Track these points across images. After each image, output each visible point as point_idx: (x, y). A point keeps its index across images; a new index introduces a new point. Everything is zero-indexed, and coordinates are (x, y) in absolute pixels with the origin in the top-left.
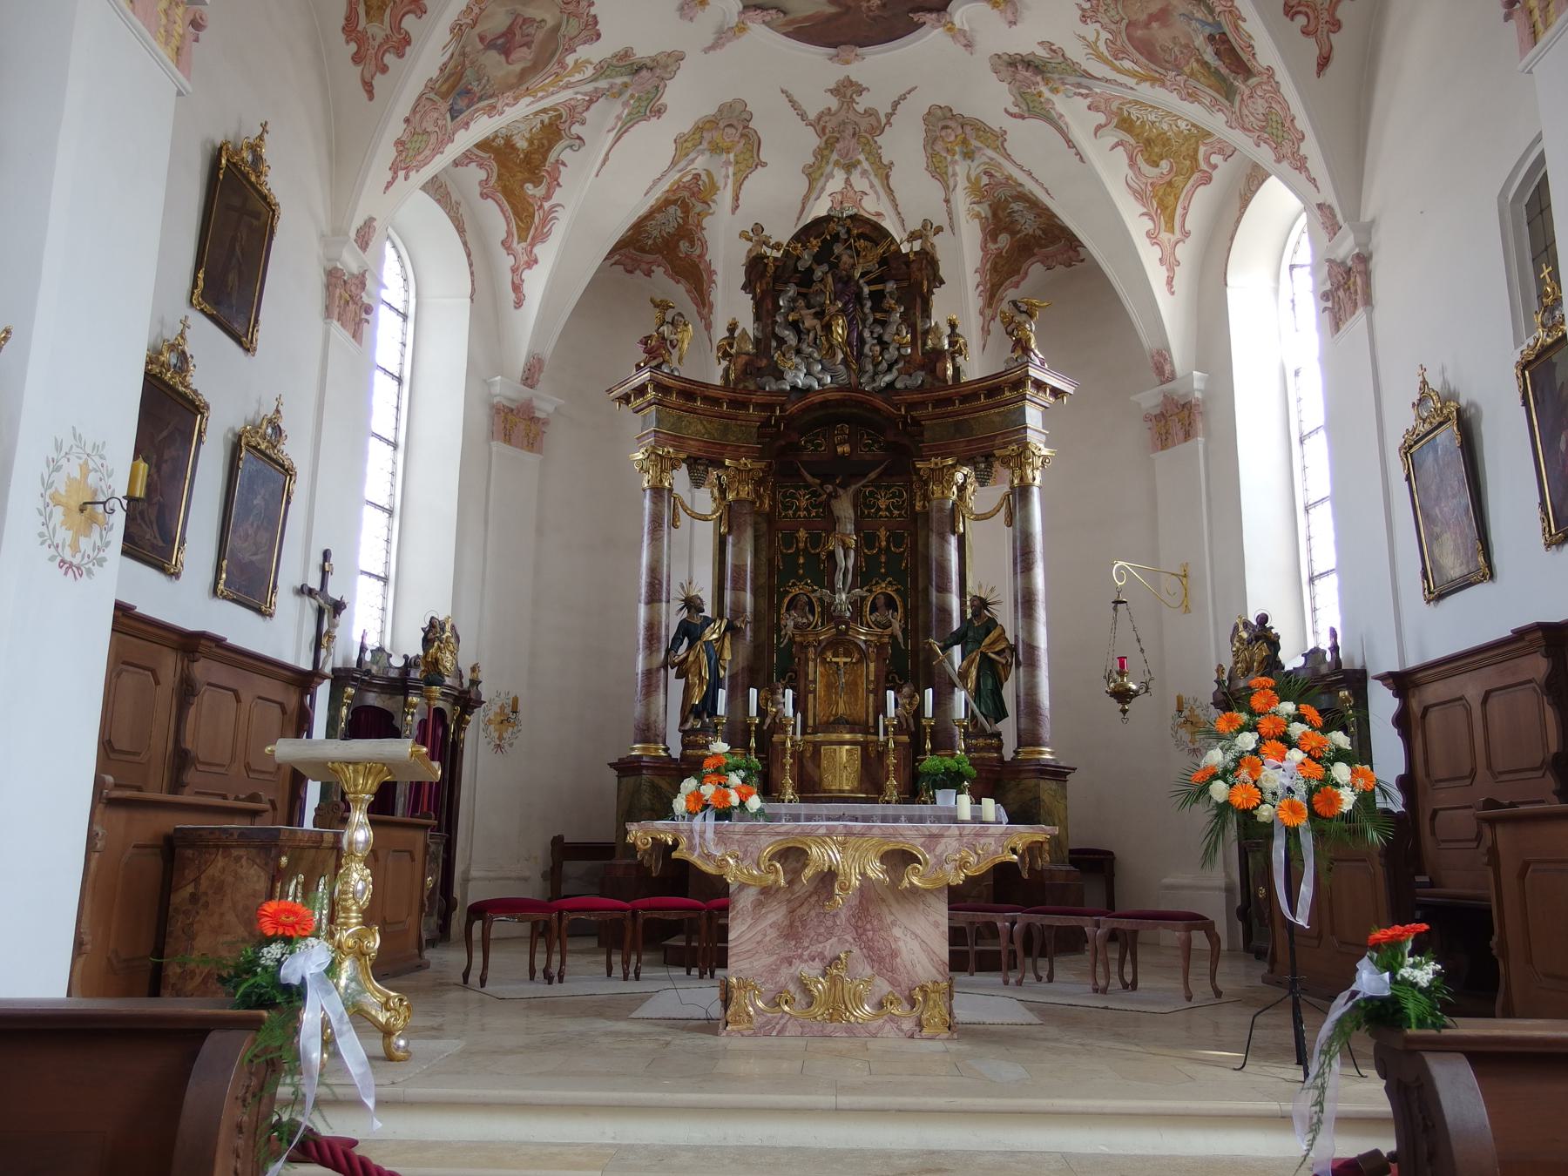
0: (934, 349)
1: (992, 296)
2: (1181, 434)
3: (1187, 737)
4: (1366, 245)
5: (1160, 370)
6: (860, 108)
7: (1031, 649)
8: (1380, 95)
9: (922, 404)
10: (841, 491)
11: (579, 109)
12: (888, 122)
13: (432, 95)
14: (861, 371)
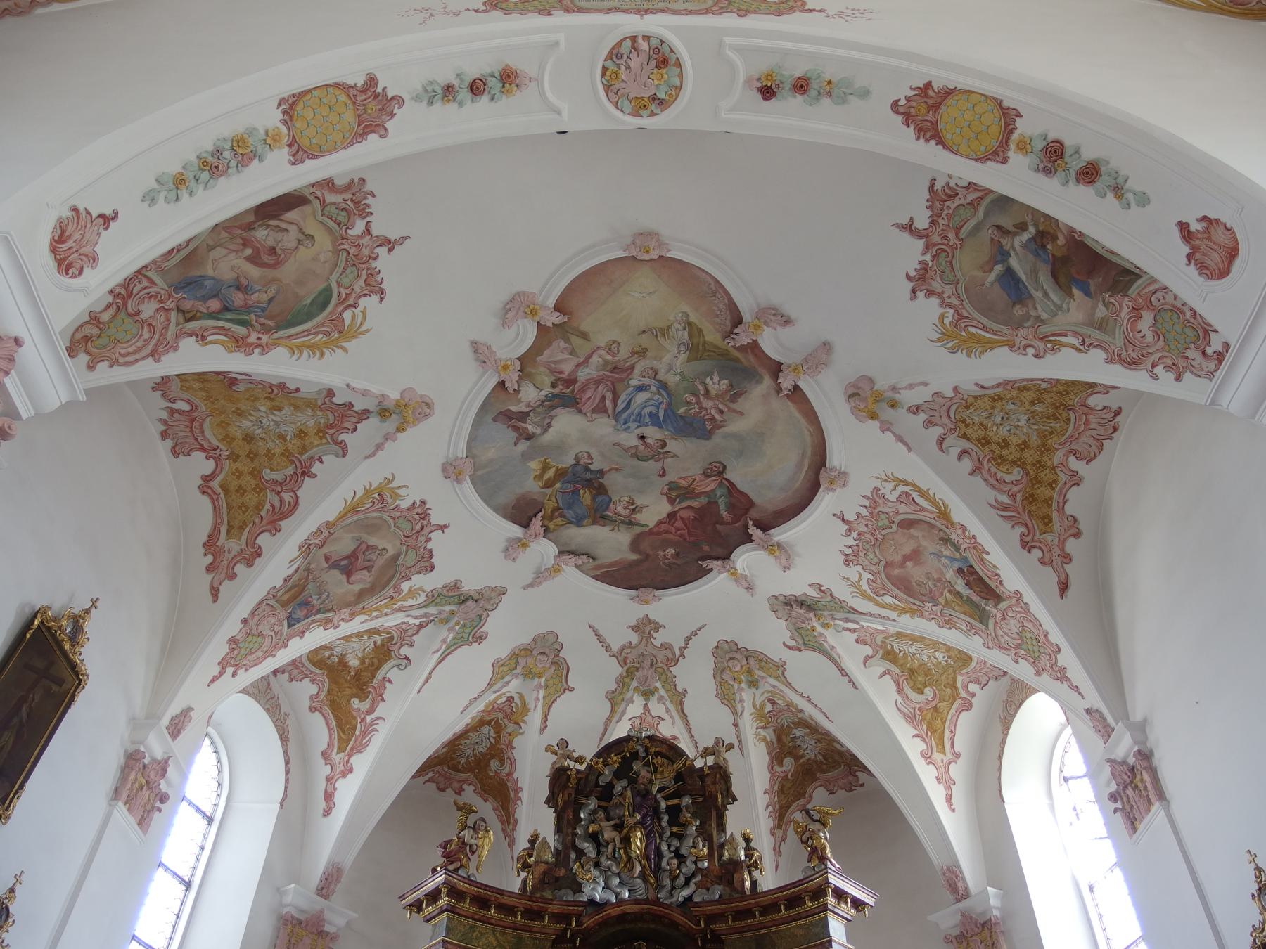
0: (730, 860)
4: (1144, 743)
5: (954, 888)
6: (657, 643)
8: (1122, 613)
9: (721, 916)
11: (409, 633)
12: (682, 655)
13: (273, 602)
14: (659, 886)
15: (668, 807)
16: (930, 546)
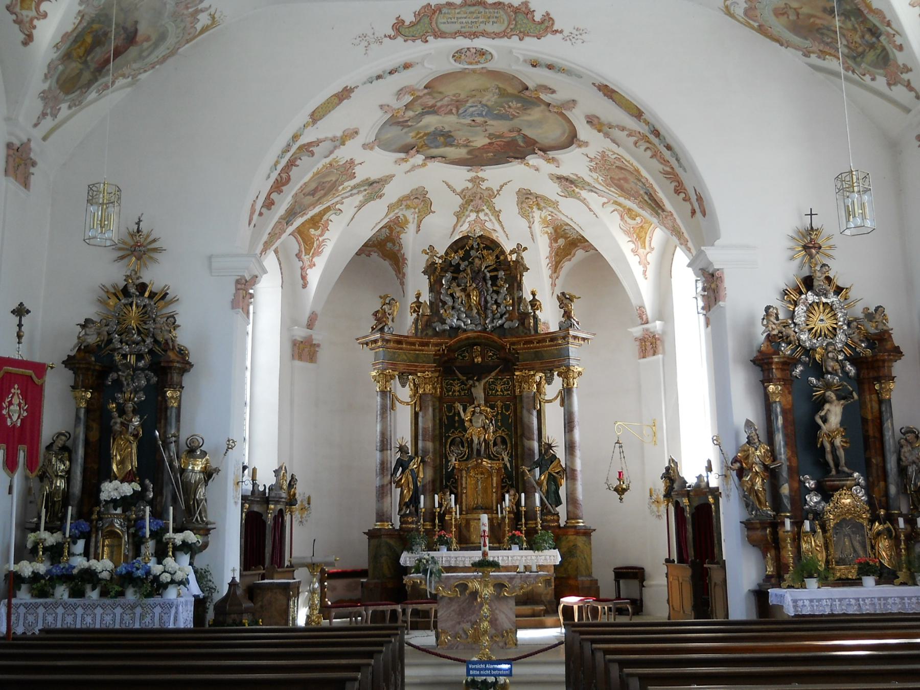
1: (556, 267)
2: (652, 351)
3: (655, 509)
7: (573, 471)
10: (477, 383)
15: (491, 277)
16: (631, 179)
